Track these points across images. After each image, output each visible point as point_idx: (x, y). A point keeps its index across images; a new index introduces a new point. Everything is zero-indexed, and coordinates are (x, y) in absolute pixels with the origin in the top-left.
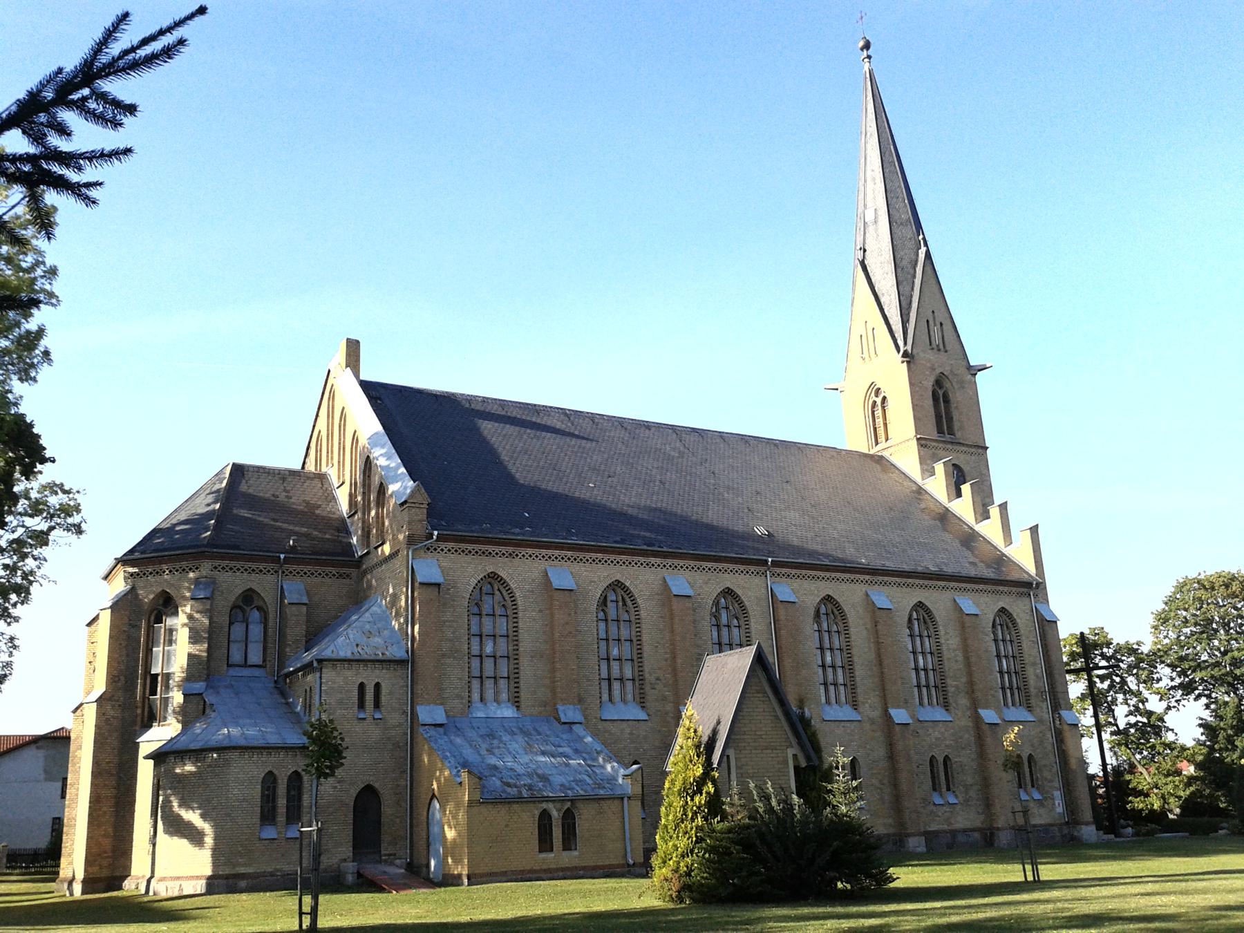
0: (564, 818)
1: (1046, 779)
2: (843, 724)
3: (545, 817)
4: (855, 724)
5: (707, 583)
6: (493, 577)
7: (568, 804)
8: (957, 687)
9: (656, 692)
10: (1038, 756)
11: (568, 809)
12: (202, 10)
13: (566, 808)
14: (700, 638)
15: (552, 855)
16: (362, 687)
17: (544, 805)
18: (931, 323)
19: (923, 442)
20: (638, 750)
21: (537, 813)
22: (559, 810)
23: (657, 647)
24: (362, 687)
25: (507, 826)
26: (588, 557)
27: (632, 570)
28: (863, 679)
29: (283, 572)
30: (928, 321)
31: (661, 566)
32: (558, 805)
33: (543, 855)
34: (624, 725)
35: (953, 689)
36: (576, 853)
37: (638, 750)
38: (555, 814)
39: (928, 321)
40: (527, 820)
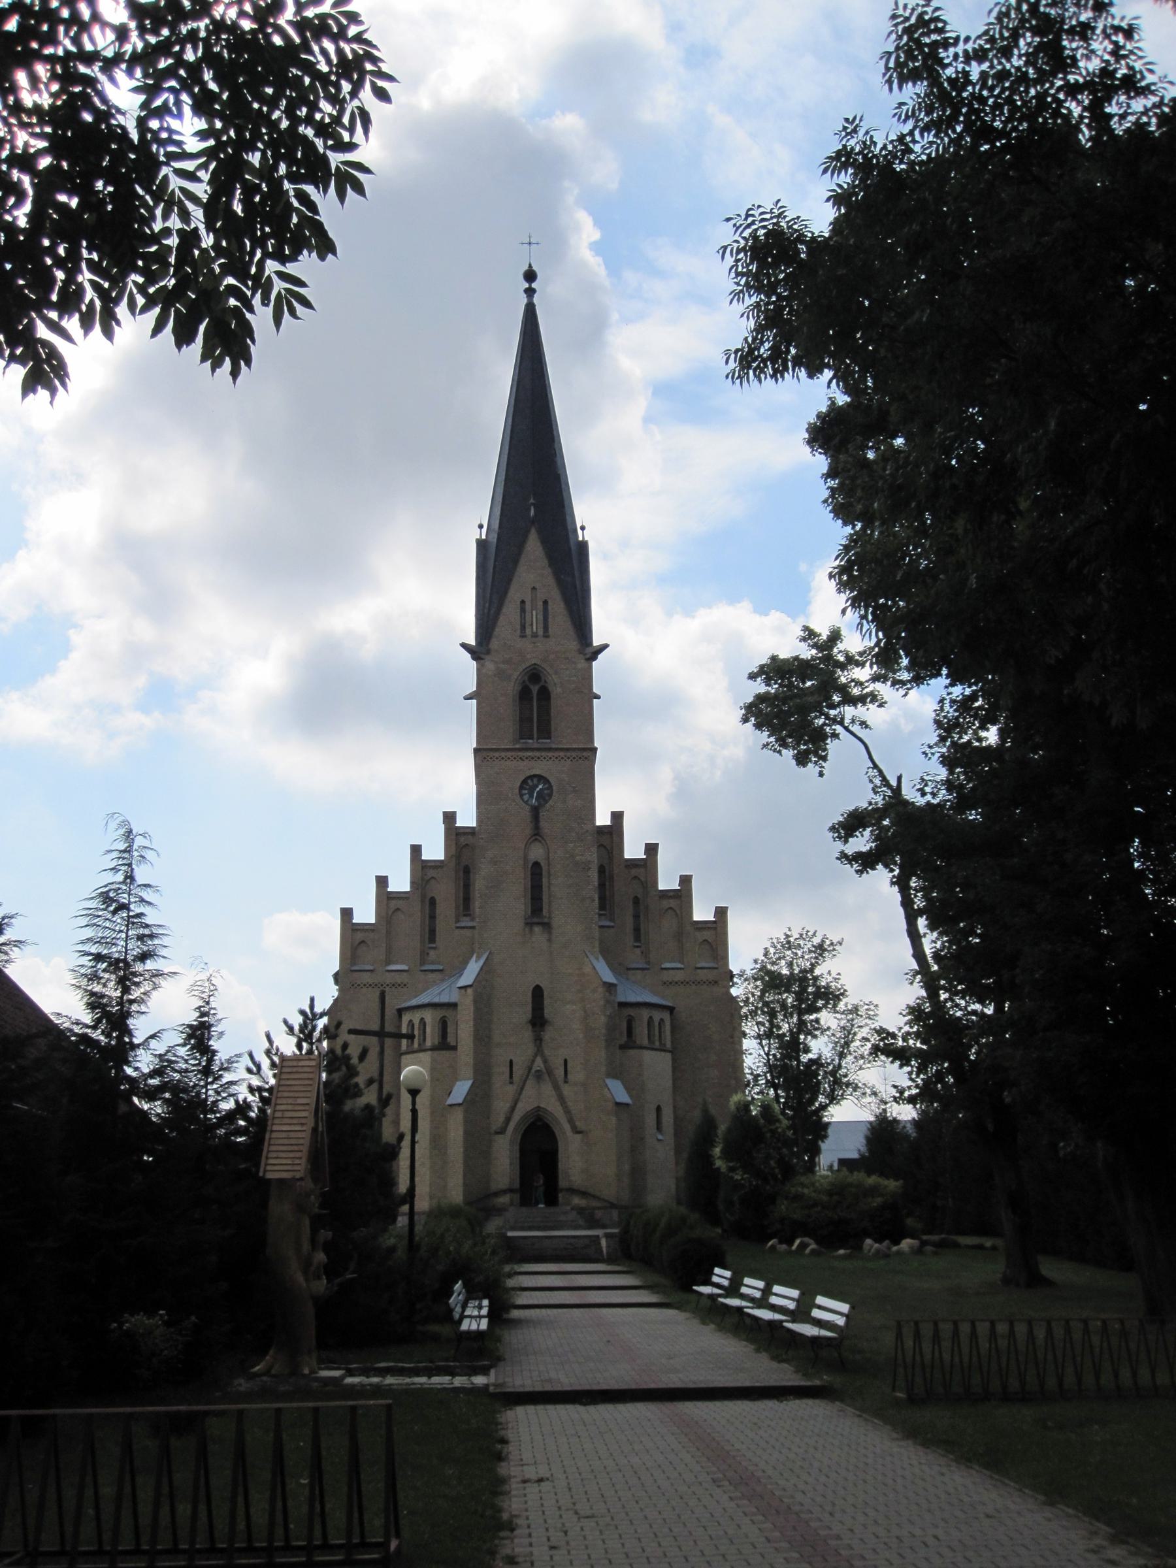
12: (530, 276)
18: (528, 606)
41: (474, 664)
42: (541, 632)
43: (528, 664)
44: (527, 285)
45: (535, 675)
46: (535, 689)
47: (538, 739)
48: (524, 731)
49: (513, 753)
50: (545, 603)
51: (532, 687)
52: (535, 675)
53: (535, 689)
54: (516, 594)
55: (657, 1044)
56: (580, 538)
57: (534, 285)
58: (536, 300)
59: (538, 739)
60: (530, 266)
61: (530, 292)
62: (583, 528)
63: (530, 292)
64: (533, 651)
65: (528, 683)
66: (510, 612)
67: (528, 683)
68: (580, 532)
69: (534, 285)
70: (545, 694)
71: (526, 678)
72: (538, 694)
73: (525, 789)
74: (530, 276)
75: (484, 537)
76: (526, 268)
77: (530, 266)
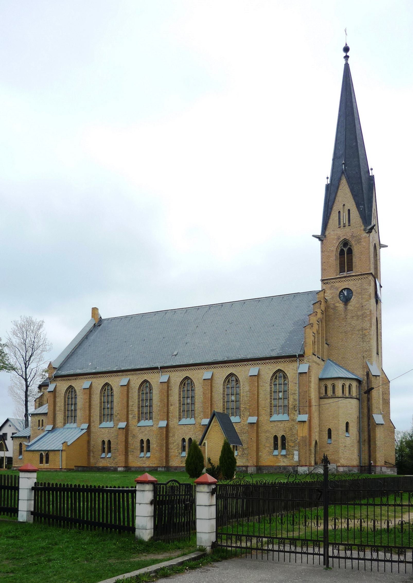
0: (46, 455)
1: (290, 446)
2: (186, 426)
3: (41, 455)
4: (192, 426)
5: (138, 379)
6: (71, 386)
7: (47, 452)
8: (245, 408)
9: (117, 418)
10: (288, 438)
11: (47, 453)
12: (346, 49)
13: (46, 453)
14: (134, 399)
15: (42, 465)
16: (39, 421)
17: (41, 452)
18: (342, 212)
19: (325, 282)
20: (110, 436)
21: (39, 454)
22: (45, 453)
23: (118, 403)
24: (39, 421)
25: (32, 457)
26: (107, 375)
27: (112, 378)
28: (198, 408)
29: (162, 372)
30: (339, 212)
31: (122, 375)
32: (45, 452)
33: (41, 465)
34: (106, 429)
35: (243, 409)
36: (48, 465)
37: (110, 436)
38: (44, 454)
39: (339, 212)
40: (37, 456)
41: (319, 242)
42: (347, 224)
43: (341, 239)
44: (345, 54)
45: (345, 243)
46: (345, 250)
47: (347, 271)
48: (342, 270)
49: (356, 277)
50: (349, 210)
51: (344, 249)
52: (345, 243)
53: (345, 250)
54: (337, 207)
55: (347, 395)
56: (371, 175)
57: (348, 54)
58: (349, 62)
59: (347, 271)
60: (346, 45)
61: (347, 57)
62: (372, 169)
63: (347, 57)
64: (344, 233)
65: (342, 248)
66: (334, 216)
67: (342, 248)
68: (370, 171)
69: (348, 54)
70: (350, 251)
71: (342, 245)
72: (347, 252)
73: (342, 295)
74: (346, 49)
75: (329, 183)
76: (344, 45)
77: (346, 45)
